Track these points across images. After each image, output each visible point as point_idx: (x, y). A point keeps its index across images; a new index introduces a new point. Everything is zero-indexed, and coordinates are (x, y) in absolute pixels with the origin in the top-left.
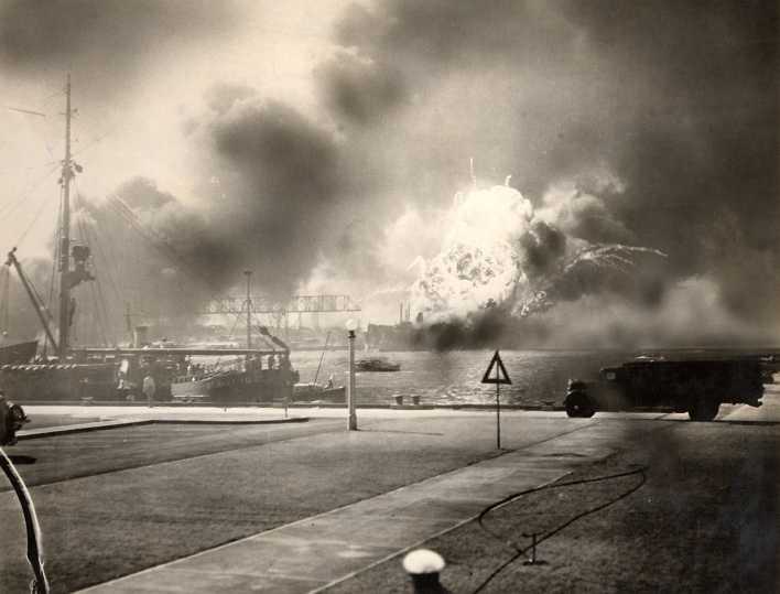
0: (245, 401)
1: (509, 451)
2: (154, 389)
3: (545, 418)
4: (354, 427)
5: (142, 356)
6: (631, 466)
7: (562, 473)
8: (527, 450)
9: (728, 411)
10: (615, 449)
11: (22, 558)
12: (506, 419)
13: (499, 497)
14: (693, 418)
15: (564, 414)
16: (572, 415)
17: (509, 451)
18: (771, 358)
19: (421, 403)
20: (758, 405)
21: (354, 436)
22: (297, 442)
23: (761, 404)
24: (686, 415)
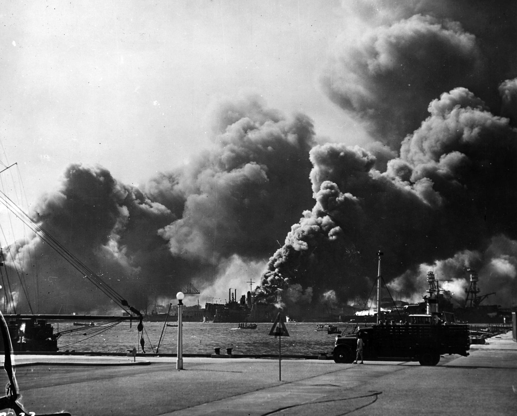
0: (7, 333)
1: (287, 383)
2: (428, 179)
3: (309, 363)
4: (181, 368)
5: (37, 319)
6: (370, 391)
7: (320, 396)
8: (300, 382)
9: (448, 360)
10: (362, 382)
11: (371, 67)
12: (284, 362)
13: (273, 409)
14: (422, 364)
15: (333, 361)
16: (338, 361)
17: (287, 383)
18: (487, 330)
19: (233, 353)
20: (467, 355)
21: (182, 374)
22: (137, 377)
23: (468, 354)
24: (418, 363)
